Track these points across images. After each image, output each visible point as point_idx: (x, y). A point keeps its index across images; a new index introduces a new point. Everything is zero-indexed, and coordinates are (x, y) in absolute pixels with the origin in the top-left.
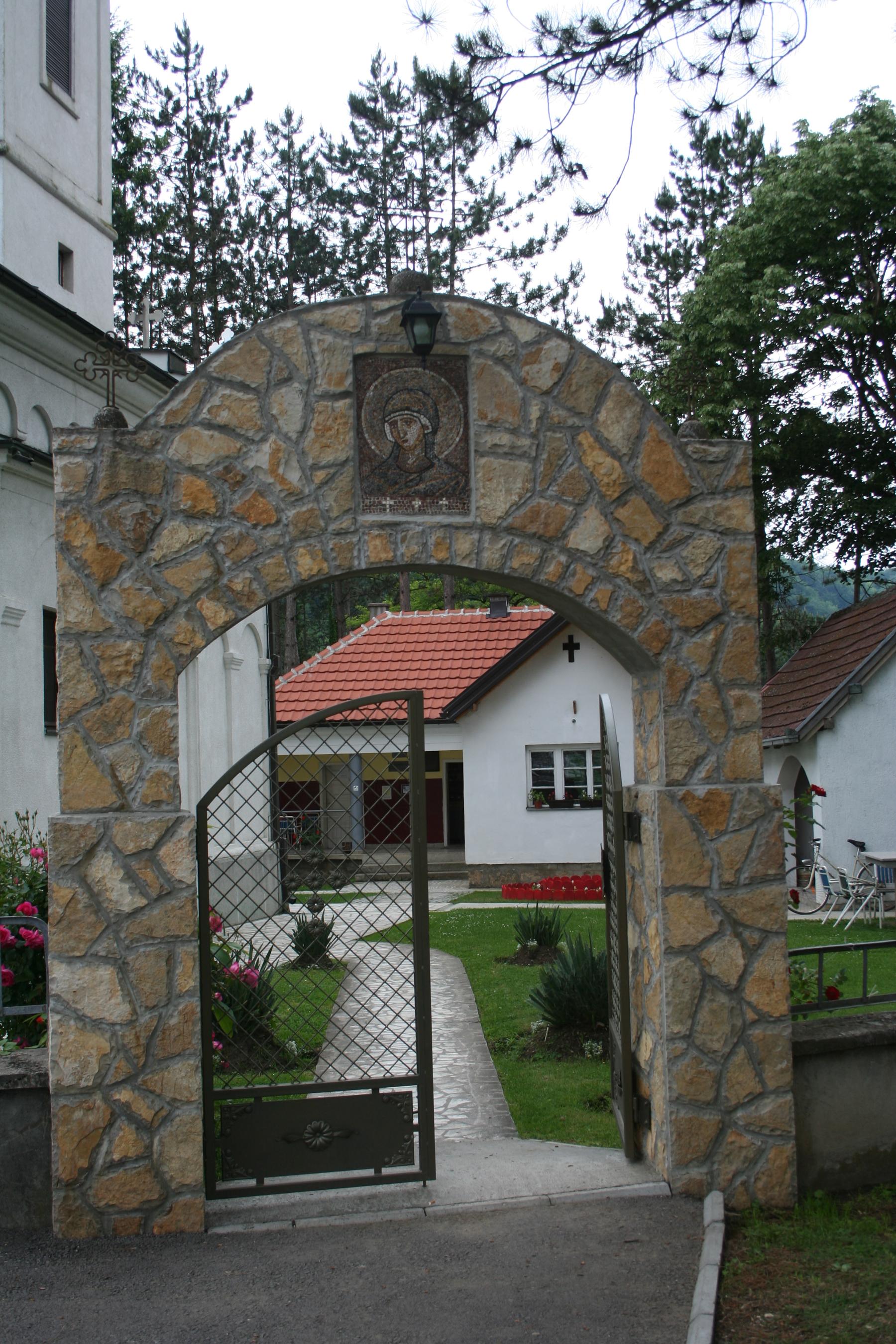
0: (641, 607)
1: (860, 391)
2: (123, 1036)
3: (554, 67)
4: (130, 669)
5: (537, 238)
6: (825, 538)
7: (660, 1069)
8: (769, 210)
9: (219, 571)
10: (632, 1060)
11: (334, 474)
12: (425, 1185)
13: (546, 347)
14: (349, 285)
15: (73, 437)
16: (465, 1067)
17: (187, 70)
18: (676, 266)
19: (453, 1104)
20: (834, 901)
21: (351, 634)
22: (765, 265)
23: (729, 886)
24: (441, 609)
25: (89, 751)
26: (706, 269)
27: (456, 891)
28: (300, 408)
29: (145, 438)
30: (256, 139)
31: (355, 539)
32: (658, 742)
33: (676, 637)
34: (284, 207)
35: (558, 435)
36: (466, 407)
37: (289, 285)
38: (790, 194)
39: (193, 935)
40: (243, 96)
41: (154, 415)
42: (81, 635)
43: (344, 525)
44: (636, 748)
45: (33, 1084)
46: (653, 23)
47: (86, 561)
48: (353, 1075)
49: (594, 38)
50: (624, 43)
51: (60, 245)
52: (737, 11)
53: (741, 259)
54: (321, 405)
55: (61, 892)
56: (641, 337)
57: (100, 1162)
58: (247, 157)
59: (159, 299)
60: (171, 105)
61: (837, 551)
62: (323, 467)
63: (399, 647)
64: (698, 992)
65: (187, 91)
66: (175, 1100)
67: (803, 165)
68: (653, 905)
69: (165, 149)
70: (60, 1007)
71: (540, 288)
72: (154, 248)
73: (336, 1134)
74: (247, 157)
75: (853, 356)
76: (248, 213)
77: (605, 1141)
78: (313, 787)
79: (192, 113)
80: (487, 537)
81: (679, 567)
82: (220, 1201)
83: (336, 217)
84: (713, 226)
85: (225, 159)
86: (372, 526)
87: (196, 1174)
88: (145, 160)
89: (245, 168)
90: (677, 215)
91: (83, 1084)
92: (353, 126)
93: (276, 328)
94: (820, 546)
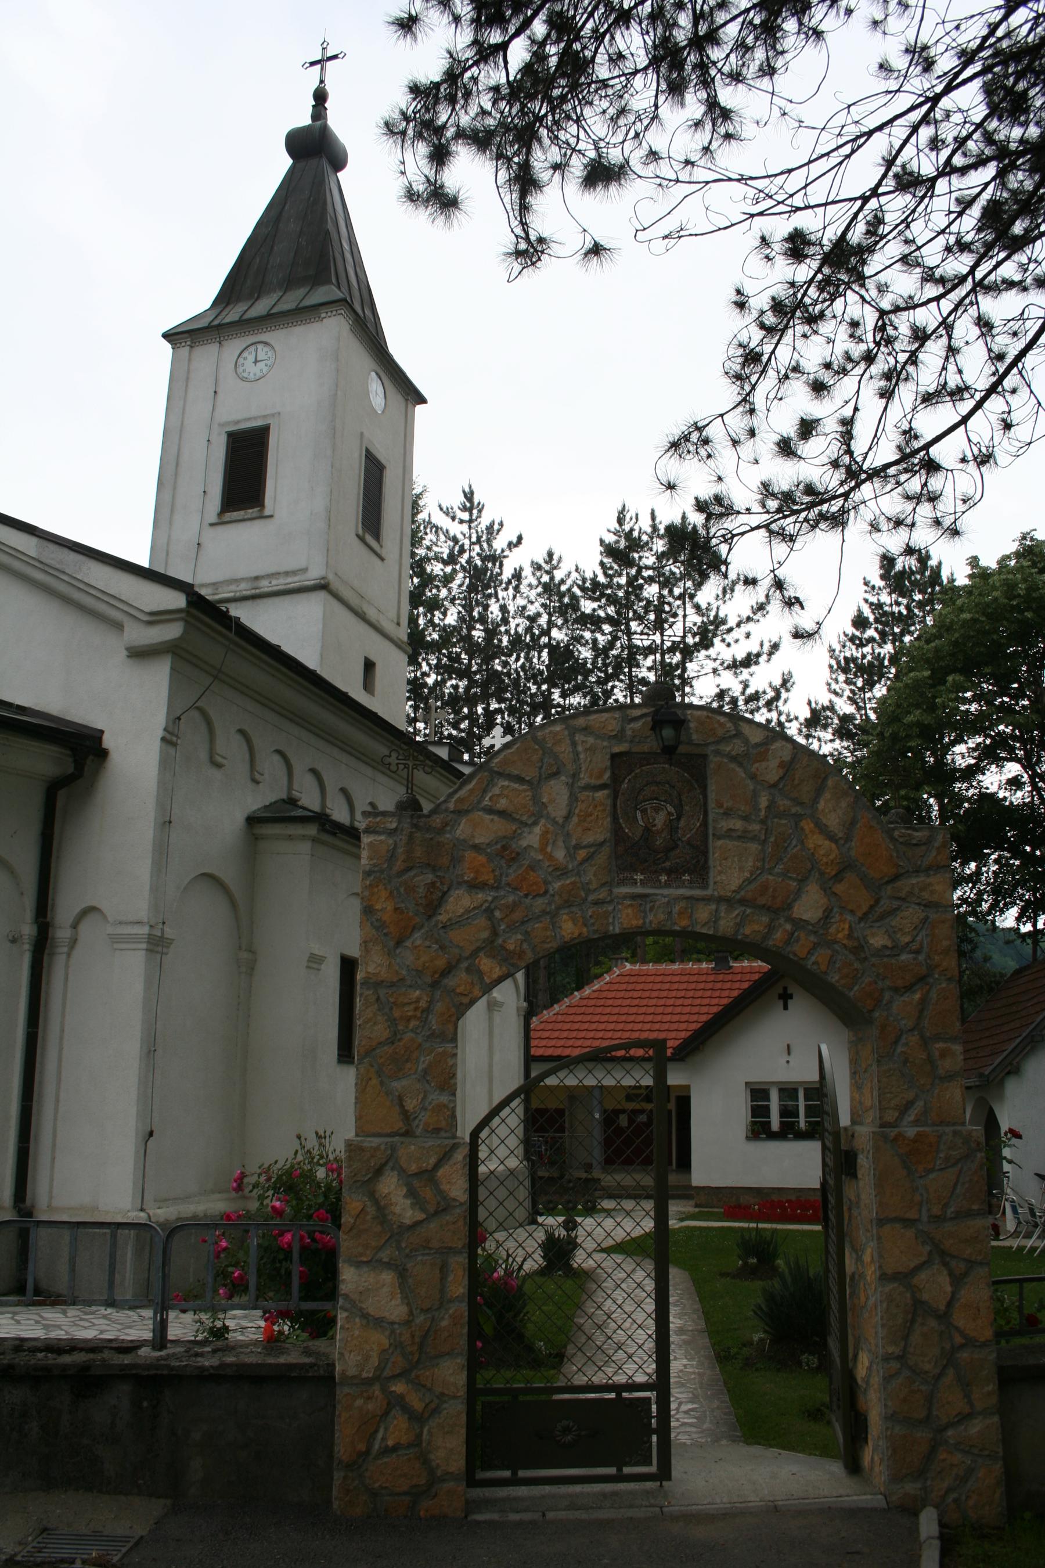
0: (856, 969)
1: (1032, 778)
2: (400, 1334)
3: (775, 521)
4: (418, 1014)
5: (755, 652)
6: (1006, 905)
7: (876, 1386)
8: (949, 629)
9: (495, 933)
10: (850, 1376)
11: (594, 853)
12: (661, 1485)
13: (773, 747)
14: (598, 690)
15: (378, 819)
16: (694, 1373)
17: (471, 521)
18: (871, 675)
19: (684, 1408)
20: (1024, 1229)
21: (595, 982)
22: (948, 674)
23: (938, 1219)
24: (673, 961)
25: (382, 1083)
26: (896, 676)
27: (683, 1209)
28: (566, 797)
29: (437, 820)
30: (524, 574)
31: (610, 908)
32: (872, 1088)
33: (887, 996)
34: (545, 627)
35: (784, 822)
36: (705, 797)
37: (549, 690)
38: (966, 616)
39: (463, 1247)
40: (515, 541)
41: (445, 801)
42: (378, 984)
43: (601, 897)
44: (852, 1092)
45: (322, 1372)
46: (858, 485)
47: (385, 922)
48: (599, 1379)
49: (807, 499)
50: (833, 502)
51: (366, 658)
52: (924, 477)
53: (927, 669)
54: (583, 796)
55: (353, 1204)
56: (842, 732)
57: (376, 1447)
58: (517, 589)
59: (442, 700)
60: (457, 548)
61: (1016, 915)
62: (585, 847)
63: (636, 994)
64: (910, 1316)
65: (470, 537)
66: (443, 1394)
67: (976, 592)
68: (869, 1234)
69: (451, 582)
70: (348, 1306)
71: (757, 692)
72: (439, 660)
73: (583, 1433)
74: (517, 589)
75: (1025, 750)
76: (516, 632)
77: (825, 1451)
78: (561, 1112)
79: (474, 554)
80: (723, 908)
81: (889, 936)
82: (478, 1489)
83: (587, 635)
84: (902, 642)
85: (499, 589)
86: (625, 897)
87: (458, 1464)
88: (434, 591)
89: (514, 597)
90: (871, 633)
91: (365, 1375)
92: (602, 564)
93: (547, 731)
94: (1002, 912)
